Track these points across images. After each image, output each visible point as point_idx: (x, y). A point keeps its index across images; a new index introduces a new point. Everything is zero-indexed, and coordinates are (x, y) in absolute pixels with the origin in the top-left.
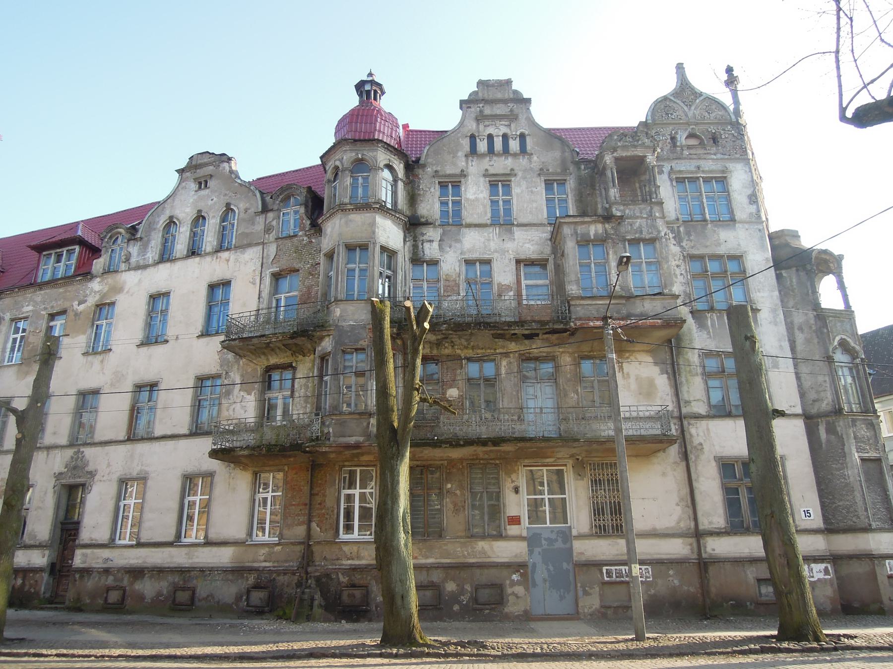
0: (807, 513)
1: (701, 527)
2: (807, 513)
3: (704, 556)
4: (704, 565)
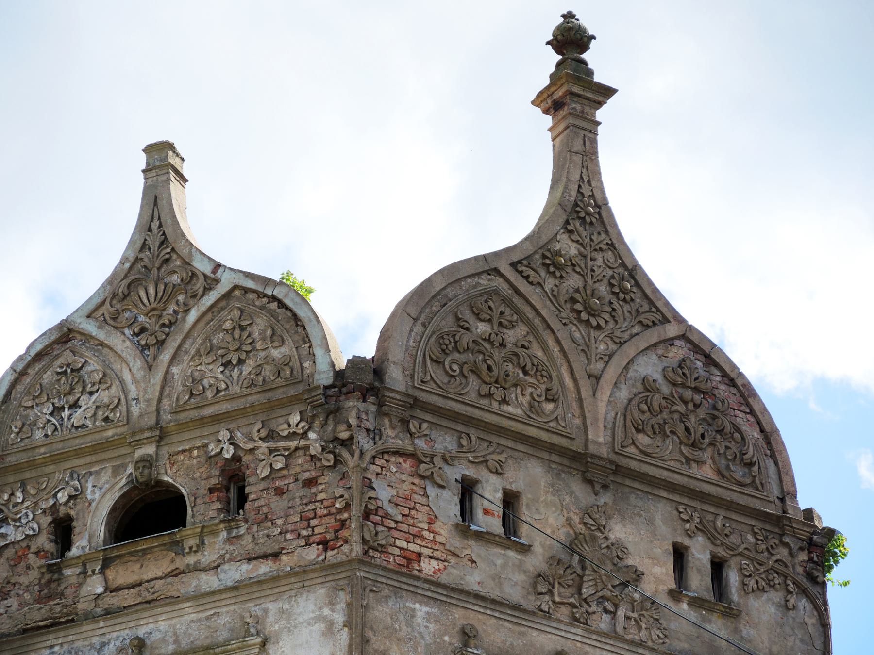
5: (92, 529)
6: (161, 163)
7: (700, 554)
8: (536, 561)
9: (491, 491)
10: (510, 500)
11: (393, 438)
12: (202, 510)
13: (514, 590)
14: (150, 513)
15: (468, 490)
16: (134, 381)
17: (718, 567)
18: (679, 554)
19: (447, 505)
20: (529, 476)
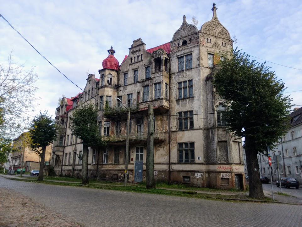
0: (199, 158)
1: (171, 162)
2: (199, 158)
3: (171, 169)
4: (170, 172)
5: (181, 44)
6: (184, 17)
7: (224, 43)
8: (212, 44)
9: (209, 39)
10: (210, 40)
11: (202, 36)
12: (188, 42)
13: (211, 46)
14: (185, 43)
15: (207, 39)
16: (184, 34)
17: (225, 44)
18: (222, 43)
19: (206, 40)
20: (212, 38)
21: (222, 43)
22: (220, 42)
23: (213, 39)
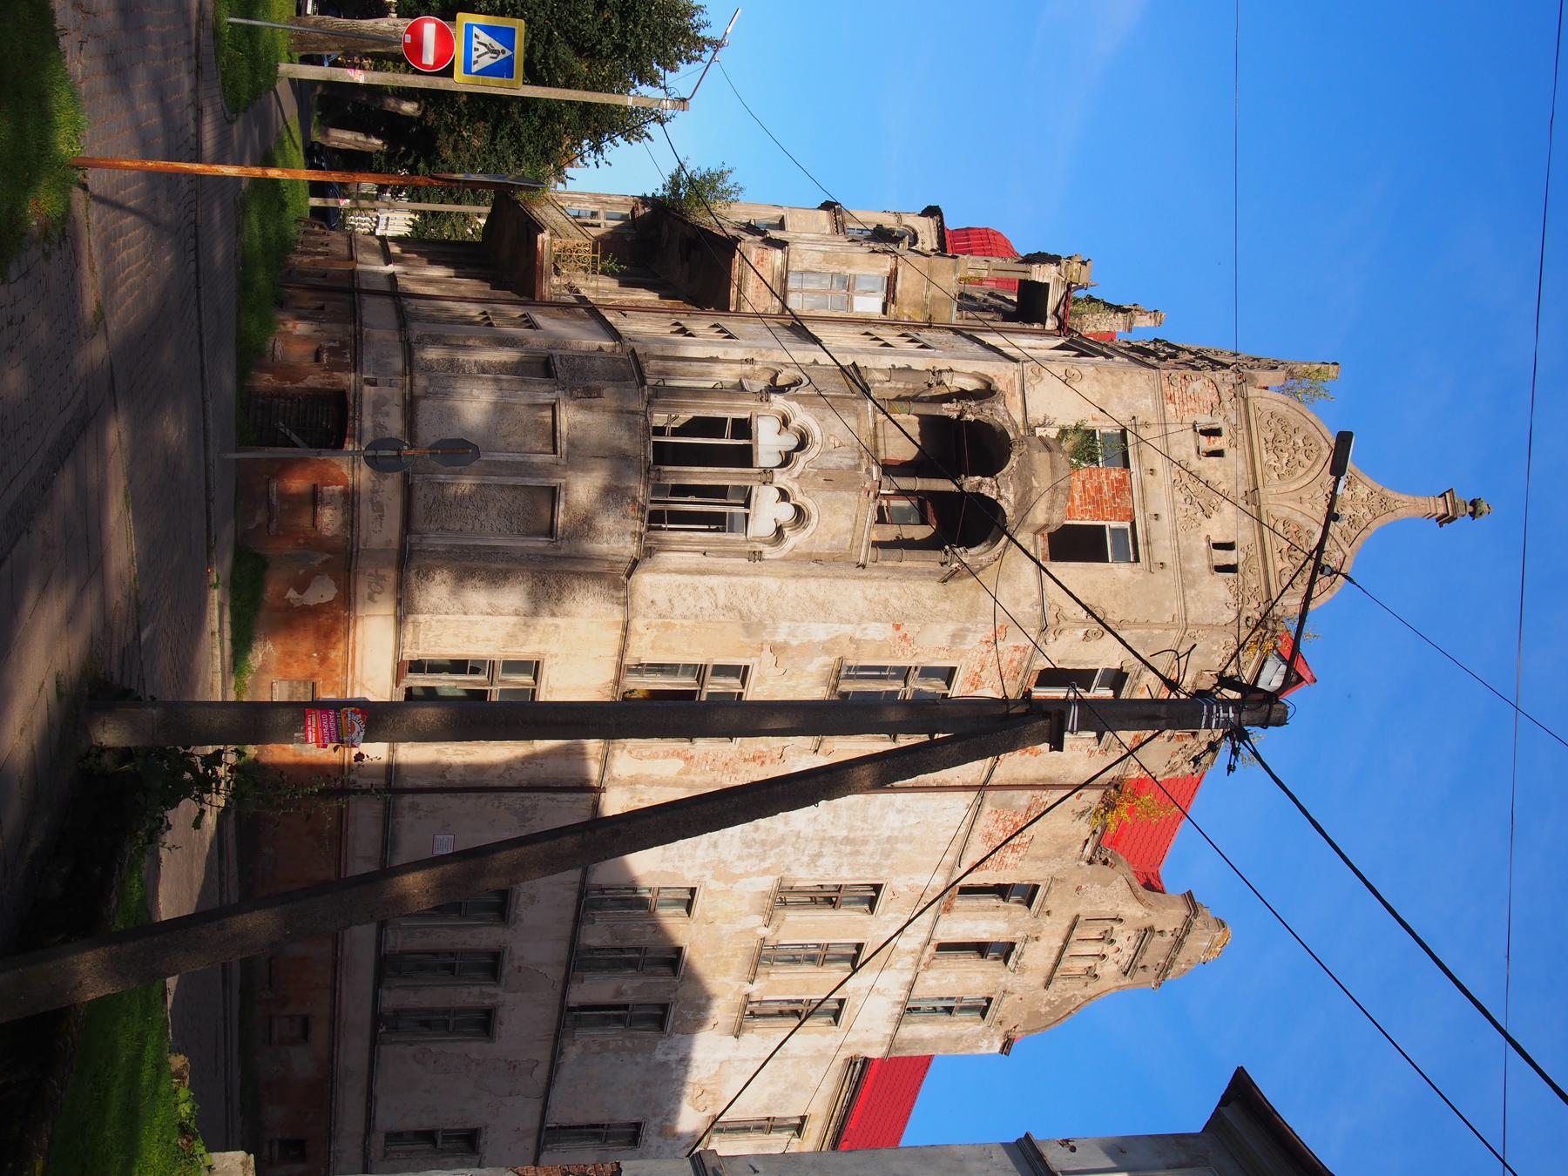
9: (1217, 443)
10: (1218, 453)
15: (1216, 432)
17: (1231, 569)
18: (1229, 546)
20: (1235, 461)
21: (1229, 546)
22: (1225, 523)
23: (1227, 473)
